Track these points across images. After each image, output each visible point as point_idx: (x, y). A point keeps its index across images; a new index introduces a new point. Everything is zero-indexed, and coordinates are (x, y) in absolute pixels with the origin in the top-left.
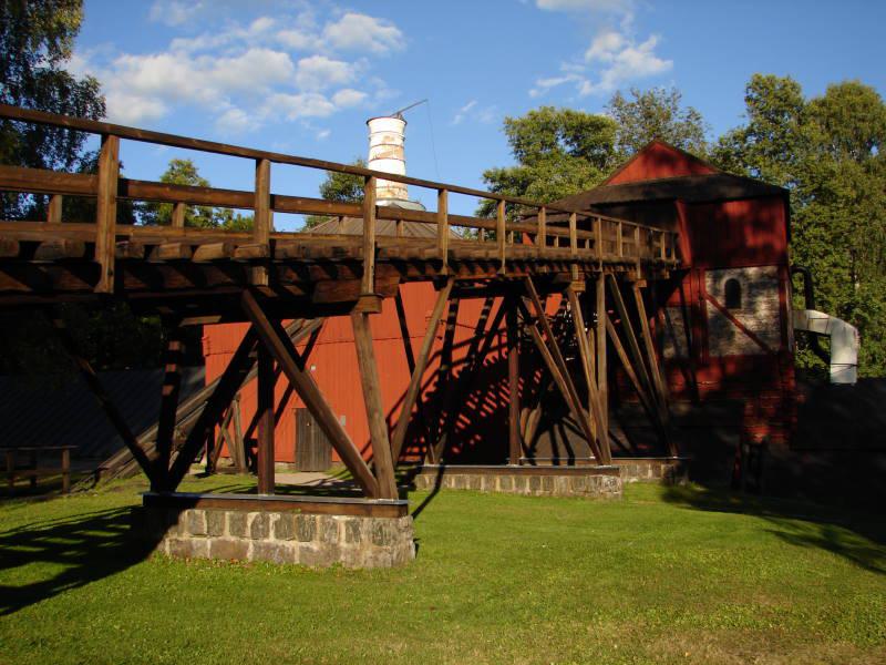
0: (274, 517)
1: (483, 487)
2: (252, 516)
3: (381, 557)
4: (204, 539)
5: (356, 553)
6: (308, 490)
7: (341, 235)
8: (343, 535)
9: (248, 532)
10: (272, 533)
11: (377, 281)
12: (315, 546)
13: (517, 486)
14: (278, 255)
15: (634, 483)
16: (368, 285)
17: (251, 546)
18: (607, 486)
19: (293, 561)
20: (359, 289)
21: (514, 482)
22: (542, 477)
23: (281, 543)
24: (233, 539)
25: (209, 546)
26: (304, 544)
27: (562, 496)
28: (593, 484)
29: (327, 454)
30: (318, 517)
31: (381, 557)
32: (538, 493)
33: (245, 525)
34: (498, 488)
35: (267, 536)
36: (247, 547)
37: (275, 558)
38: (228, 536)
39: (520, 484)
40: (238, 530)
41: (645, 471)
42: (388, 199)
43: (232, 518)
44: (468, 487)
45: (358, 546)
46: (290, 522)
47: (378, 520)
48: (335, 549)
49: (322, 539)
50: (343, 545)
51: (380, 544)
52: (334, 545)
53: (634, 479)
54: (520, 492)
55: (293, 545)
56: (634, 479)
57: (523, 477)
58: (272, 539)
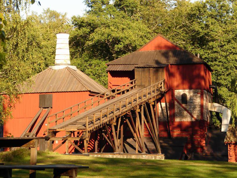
22: (129, 156)
25: (188, 157)
42: (65, 64)
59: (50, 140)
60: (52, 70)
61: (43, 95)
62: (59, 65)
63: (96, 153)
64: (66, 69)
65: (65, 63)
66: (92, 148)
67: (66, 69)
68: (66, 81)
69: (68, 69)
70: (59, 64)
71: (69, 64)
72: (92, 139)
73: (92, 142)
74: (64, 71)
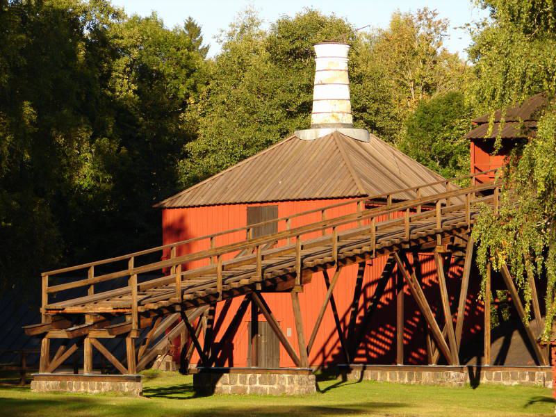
0: (259, 376)
1: (378, 379)
2: (249, 376)
3: (301, 390)
4: (228, 386)
5: (292, 389)
6: (365, 158)
7: (287, 231)
8: (287, 382)
9: (248, 382)
10: (258, 382)
11: (303, 271)
12: (275, 386)
13: (400, 378)
14: (265, 278)
15: (516, 385)
16: (298, 281)
17: (249, 389)
18: (453, 378)
19: (266, 393)
20: (294, 282)
21: (398, 376)
22: (415, 373)
23: (263, 386)
24: (241, 385)
25: (230, 389)
26: (271, 386)
27: (426, 384)
28: (445, 376)
29: (275, 361)
30: (277, 375)
31: (301, 390)
32: (412, 382)
33: (246, 379)
34: (388, 380)
35: (255, 383)
36: (247, 388)
37: (259, 392)
38: (239, 384)
39: (402, 377)
40: (243, 382)
41: (523, 376)
42: (333, 125)
43: (240, 376)
44: (370, 379)
45: (293, 386)
46: (265, 377)
47: (301, 375)
48: (284, 387)
49: (278, 384)
50: (287, 386)
51: (301, 385)
52: (283, 386)
53: (516, 383)
54: (402, 382)
55: (267, 387)
56: (516, 383)
57: (404, 372)
58: (258, 384)
59: (47, 336)
60: (298, 140)
61: (256, 207)
62: (318, 126)
63: (399, 365)
64: (330, 138)
65: (333, 121)
66: (387, 348)
67: (330, 138)
68: (325, 163)
69: (337, 137)
70: (317, 125)
71: (346, 126)
72: (388, 326)
73: (388, 333)
74: (323, 143)
